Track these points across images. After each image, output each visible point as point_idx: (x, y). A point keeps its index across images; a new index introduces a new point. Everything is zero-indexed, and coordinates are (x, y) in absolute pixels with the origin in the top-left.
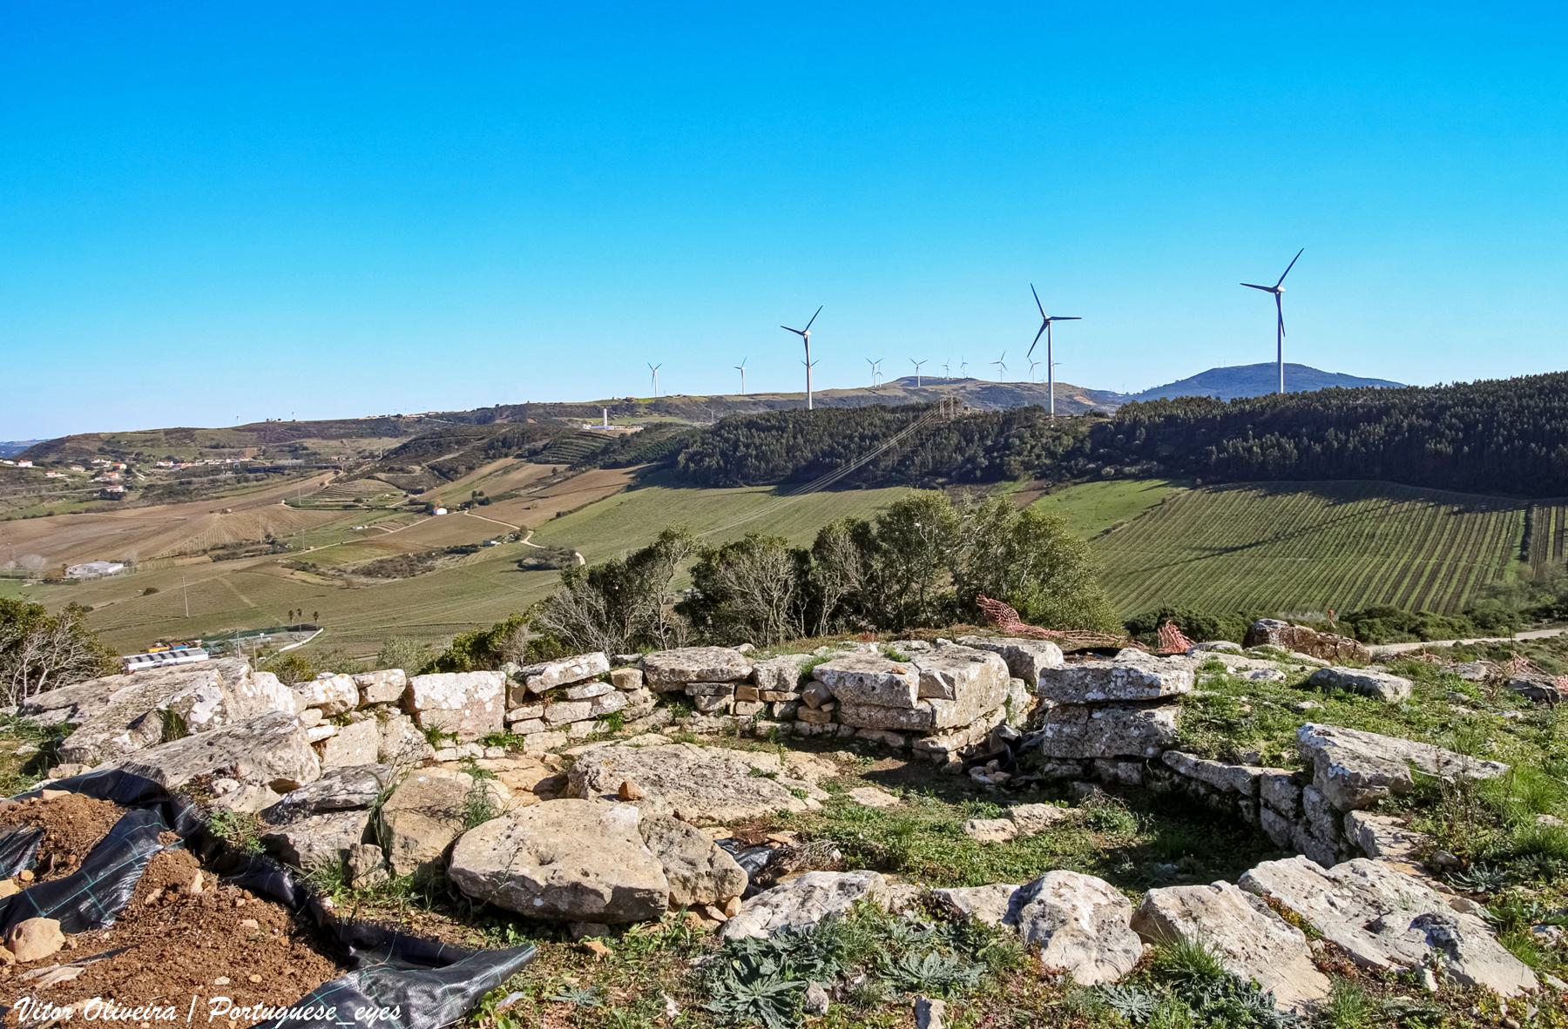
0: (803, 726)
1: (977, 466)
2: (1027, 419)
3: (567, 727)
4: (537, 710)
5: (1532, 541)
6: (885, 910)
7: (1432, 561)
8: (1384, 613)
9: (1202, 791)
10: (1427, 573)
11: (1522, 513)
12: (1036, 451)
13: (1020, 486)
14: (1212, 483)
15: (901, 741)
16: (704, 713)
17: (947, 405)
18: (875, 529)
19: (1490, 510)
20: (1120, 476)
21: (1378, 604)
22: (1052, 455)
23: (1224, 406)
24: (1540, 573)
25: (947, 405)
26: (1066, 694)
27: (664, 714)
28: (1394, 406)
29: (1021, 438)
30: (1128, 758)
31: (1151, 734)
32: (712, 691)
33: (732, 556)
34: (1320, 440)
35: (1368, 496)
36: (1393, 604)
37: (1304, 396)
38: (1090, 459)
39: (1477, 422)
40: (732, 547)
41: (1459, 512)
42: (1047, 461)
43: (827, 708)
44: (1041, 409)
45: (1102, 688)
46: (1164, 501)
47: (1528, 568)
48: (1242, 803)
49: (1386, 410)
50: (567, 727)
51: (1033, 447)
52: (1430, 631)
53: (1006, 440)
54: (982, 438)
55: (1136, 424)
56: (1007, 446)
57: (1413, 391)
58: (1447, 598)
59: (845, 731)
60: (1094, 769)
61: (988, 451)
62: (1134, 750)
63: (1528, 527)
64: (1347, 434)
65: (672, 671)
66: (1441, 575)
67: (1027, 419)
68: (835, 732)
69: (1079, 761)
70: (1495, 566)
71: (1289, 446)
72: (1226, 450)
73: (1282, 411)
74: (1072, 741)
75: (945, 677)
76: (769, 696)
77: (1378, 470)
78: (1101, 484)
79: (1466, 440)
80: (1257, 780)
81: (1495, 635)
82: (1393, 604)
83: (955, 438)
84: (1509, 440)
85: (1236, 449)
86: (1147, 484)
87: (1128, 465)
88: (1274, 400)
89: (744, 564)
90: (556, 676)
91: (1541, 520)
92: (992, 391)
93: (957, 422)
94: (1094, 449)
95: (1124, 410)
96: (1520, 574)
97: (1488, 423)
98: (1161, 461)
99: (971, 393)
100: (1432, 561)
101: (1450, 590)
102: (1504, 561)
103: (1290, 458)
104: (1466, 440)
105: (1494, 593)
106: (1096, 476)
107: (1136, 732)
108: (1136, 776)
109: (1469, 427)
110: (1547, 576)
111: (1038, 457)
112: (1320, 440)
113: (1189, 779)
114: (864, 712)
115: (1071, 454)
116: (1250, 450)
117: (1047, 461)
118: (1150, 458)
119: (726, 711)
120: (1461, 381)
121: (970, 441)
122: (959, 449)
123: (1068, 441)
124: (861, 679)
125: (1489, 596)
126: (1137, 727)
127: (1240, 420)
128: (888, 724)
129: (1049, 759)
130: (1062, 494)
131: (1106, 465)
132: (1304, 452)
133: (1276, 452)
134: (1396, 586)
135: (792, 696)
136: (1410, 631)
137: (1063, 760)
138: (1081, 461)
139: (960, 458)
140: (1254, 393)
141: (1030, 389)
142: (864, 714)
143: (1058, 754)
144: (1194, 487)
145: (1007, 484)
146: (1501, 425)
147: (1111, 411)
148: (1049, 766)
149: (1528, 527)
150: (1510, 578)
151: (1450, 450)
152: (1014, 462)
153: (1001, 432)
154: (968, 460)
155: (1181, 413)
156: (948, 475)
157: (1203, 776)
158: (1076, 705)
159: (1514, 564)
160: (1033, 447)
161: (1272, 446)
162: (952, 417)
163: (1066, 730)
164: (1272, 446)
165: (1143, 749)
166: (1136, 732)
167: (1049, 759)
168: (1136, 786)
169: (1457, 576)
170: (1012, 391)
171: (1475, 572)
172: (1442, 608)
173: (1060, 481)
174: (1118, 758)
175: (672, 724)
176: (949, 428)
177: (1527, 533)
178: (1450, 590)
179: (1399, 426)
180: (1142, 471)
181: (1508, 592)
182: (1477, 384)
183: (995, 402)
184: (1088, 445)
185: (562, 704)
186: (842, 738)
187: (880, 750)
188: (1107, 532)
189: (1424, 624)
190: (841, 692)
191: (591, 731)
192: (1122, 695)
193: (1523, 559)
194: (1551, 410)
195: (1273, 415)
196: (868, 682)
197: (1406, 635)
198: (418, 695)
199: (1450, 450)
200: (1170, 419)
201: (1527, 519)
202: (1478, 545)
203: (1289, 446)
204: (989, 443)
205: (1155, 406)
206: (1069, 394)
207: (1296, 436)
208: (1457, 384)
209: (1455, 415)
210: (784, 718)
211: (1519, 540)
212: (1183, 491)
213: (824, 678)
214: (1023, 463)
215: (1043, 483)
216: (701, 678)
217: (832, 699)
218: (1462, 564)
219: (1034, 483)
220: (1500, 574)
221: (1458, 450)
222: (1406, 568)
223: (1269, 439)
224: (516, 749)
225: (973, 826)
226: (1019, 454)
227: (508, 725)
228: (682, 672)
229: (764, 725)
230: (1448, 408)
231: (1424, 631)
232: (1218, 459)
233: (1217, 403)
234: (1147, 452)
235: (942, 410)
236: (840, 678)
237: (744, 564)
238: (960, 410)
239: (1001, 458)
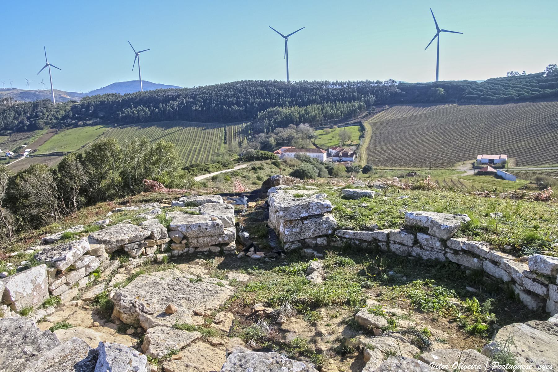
0: (175, 252)
1: (24, 125)
2: (44, 104)
3: (77, 284)
4: (63, 279)
5: (227, 137)
6: (515, 338)
7: (199, 146)
8: (197, 165)
9: (357, 242)
10: (197, 151)
11: (223, 129)
12: (50, 117)
13: (45, 131)
14: (121, 125)
15: (218, 249)
16: (134, 258)
17: (7, 100)
18: (84, 156)
19: (214, 128)
20: (85, 125)
21: (193, 163)
22: (57, 118)
23: (122, 96)
24: (231, 147)
25: (7, 100)
26: (292, 216)
27: (117, 263)
28: (181, 95)
29: (42, 112)
30: (320, 236)
31: (329, 225)
32: (136, 247)
33: (26, 176)
34: (158, 107)
35: (175, 126)
36: (198, 162)
37: (150, 92)
38: (73, 118)
39: (207, 99)
40: (25, 172)
41: (205, 129)
42: (55, 121)
43: (184, 242)
44: (49, 100)
45: (307, 211)
46: (104, 133)
47: (227, 146)
48: (380, 244)
49: (178, 96)
50: (77, 284)
51: (48, 116)
52: (210, 170)
53: (36, 113)
54: (25, 113)
55: (89, 104)
56: (37, 116)
57: (186, 89)
58: (205, 158)
59: (192, 250)
60: (305, 243)
61: (29, 118)
62: (324, 233)
63: (225, 133)
64: (166, 105)
65: (118, 241)
66: (202, 151)
67: (44, 104)
68: (188, 252)
69: (299, 241)
70: (217, 146)
71: (147, 110)
72: (124, 113)
73: (143, 98)
74: (297, 234)
75: (228, 218)
76: (159, 242)
77: (177, 117)
78: (78, 128)
79: (204, 106)
80: (388, 235)
81: (229, 169)
82: (198, 162)
83: (13, 114)
84: (217, 105)
85: (128, 112)
86: (96, 127)
87: (88, 120)
88: (140, 94)
89: (33, 179)
90: (72, 258)
91: (229, 130)
92: (25, 94)
93: (13, 107)
94: (73, 115)
95: (84, 99)
96: (225, 148)
97: (210, 100)
98: (101, 118)
99: (16, 94)
100: (199, 146)
101: (205, 155)
102: (220, 144)
103: (148, 114)
104: (204, 106)
105: (219, 155)
106: (76, 126)
107: (325, 226)
108: (325, 242)
109: (205, 101)
110: (233, 148)
111: (51, 119)
112: (158, 107)
113: (350, 239)
114: (201, 240)
115: (64, 118)
116: (133, 112)
117: (55, 121)
118: (96, 117)
119: (142, 254)
120: (201, 86)
121: (20, 115)
122: (15, 118)
123: (63, 113)
124: (199, 226)
125: (217, 156)
126: (325, 224)
127: (128, 102)
128: (213, 243)
129: (285, 243)
130: (63, 134)
131: (79, 121)
132: (152, 112)
133: (142, 113)
134: (188, 156)
135: (167, 240)
136: (205, 171)
137: (292, 243)
138: (69, 120)
139: (16, 122)
140: (132, 91)
141: (42, 92)
142: (201, 241)
143: (291, 240)
144: (114, 127)
145: (38, 131)
146: (214, 100)
147: (79, 101)
148: (287, 246)
149: (225, 133)
150: (222, 150)
151: (200, 109)
152: (41, 122)
153: (33, 110)
154: (20, 123)
155: (106, 100)
156: (12, 129)
157: (358, 237)
158: (296, 220)
159: (223, 145)
160: (48, 116)
161: (141, 111)
162: (10, 105)
163: (294, 230)
164: (141, 111)
165: (327, 232)
166: (325, 226)
167: (285, 243)
168: (325, 246)
169: (206, 151)
170: (34, 94)
171: (212, 149)
172: (203, 161)
173: (61, 128)
174: (317, 237)
175: (121, 267)
176: (9, 110)
177: (226, 135)
178: (205, 155)
179: (183, 102)
180: (94, 122)
181: (223, 154)
182: (489, 82)
183: (28, 98)
184: (71, 114)
185: (74, 272)
186: (192, 254)
187: (209, 255)
188: (83, 147)
189: (209, 168)
190: (190, 233)
191: (87, 282)
192: (316, 213)
193: (225, 143)
194: (228, 95)
195: (140, 99)
196: (203, 227)
197: (204, 172)
198: (12, 293)
199: (200, 109)
200: (102, 102)
201: (225, 130)
202: (211, 140)
203: (147, 110)
204: (29, 115)
205: (96, 97)
206: (59, 94)
207: (149, 107)
208: (200, 87)
209: (200, 97)
210: (166, 251)
211: (223, 137)
212: (110, 129)
213: (180, 229)
214: (44, 122)
215: (54, 130)
216: (131, 241)
217: (185, 237)
218: (208, 146)
219: (50, 130)
220: (219, 149)
221: (202, 109)
222: (191, 149)
223: (139, 108)
224: (59, 305)
225: (312, 278)
226: (43, 119)
227: (50, 293)
228: (122, 240)
229: (160, 256)
230: (198, 95)
231: (209, 170)
232: (122, 116)
233: (119, 96)
234: (94, 115)
235: (5, 102)
236: (188, 227)
237: (33, 179)
238: (13, 102)
239: (35, 121)
